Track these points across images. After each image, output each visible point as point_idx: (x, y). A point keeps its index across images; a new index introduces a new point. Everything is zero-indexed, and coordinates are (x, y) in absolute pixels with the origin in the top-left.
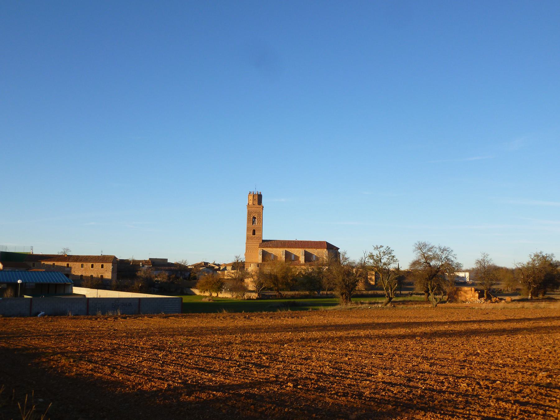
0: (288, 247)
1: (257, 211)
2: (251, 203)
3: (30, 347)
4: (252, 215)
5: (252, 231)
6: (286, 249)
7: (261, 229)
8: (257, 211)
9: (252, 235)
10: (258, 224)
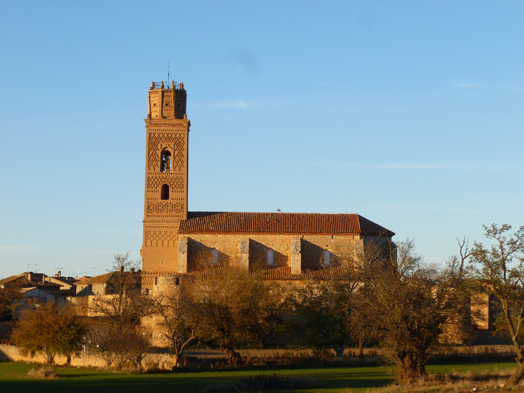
0: (259, 231)
1: (173, 136)
4: (159, 147)
5: (160, 189)
6: (188, 235)
8: (173, 136)
9: (160, 200)
10: (177, 169)
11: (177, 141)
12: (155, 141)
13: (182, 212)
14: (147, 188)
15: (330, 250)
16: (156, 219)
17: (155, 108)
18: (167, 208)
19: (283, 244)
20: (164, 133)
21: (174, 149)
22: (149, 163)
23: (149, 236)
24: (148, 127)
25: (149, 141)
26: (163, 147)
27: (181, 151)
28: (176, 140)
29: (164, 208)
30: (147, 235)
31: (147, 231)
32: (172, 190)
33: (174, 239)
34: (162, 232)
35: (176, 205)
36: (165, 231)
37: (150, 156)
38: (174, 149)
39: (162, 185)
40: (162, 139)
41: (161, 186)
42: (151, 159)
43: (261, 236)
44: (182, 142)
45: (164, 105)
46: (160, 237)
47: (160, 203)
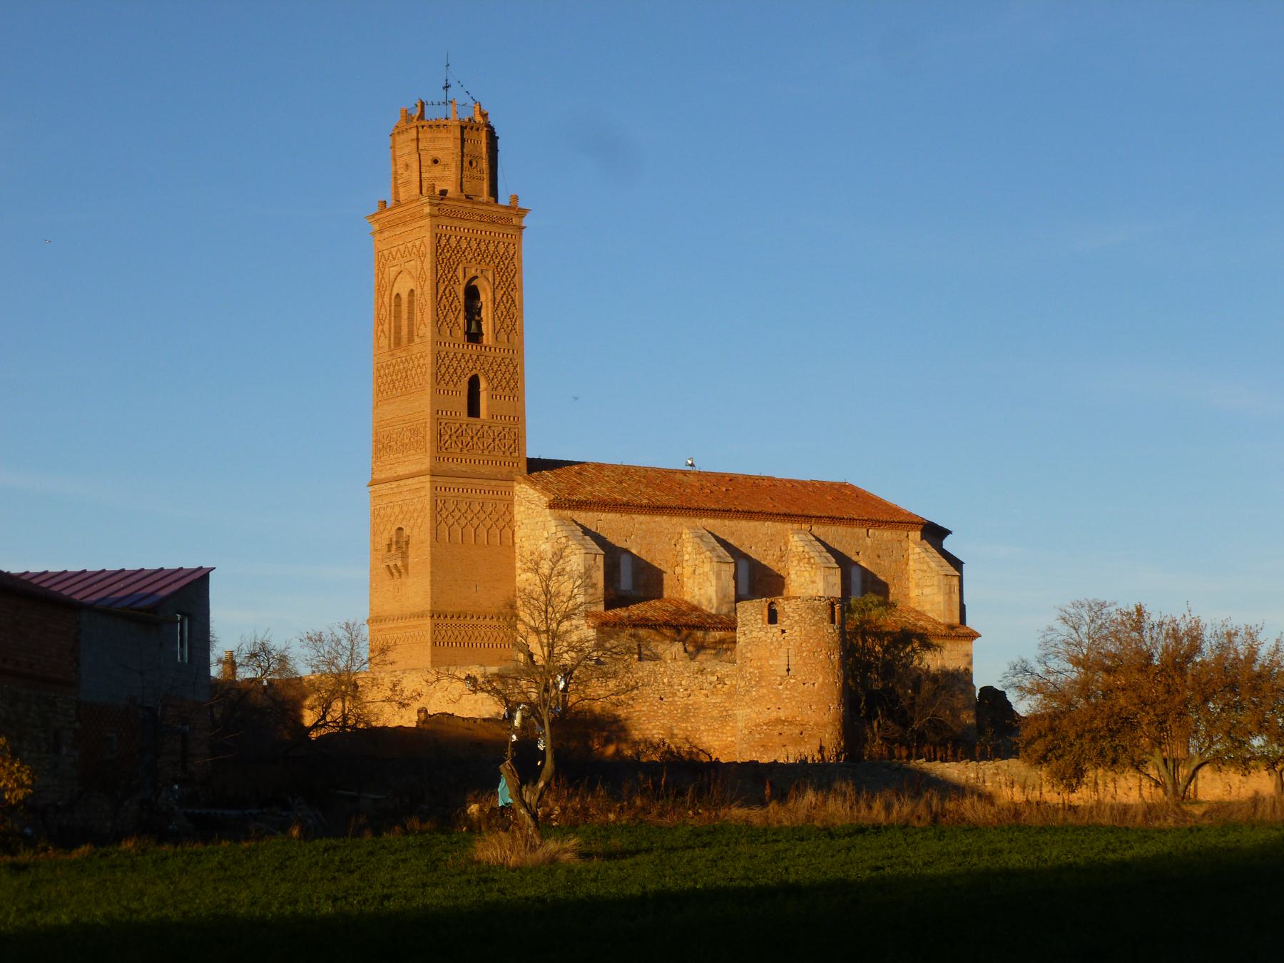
2: (448, 179)
3: (517, 723)
4: (460, 273)
7: (512, 384)
8: (491, 248)
10: (503, 336)
11: (499, 263)
12: (450, 257)
13: (517, 454)
14: (435, 384)
15: (863, 564)
16: (459, 468)
17: (437, 170)
18: (503, 441)
19: (771, 546)
20: (461, 238)
21: (494, 284)
22: (437, 315)
23: (444, 514)
24: (434, 219)
25: (437, 255)
26: (469, 276)
27: (510, 289)
28: (497, 261)
29: (475, 439)
30: (438, 509)
31: (439, 502)
32: (492, 393)
33: (501, 524)
34: (472, 503)
35: (502, 434)
36: (481, 501)
37: (439, 296)
38: (494, 284)
39: (469, 376)
40: (466, 254)
41: (467, 379)
42: (442, 305)
43: (727, 522)
44: (511, 267)
45: (466, 164)
46: (469, 518)
47: (464, 426)
